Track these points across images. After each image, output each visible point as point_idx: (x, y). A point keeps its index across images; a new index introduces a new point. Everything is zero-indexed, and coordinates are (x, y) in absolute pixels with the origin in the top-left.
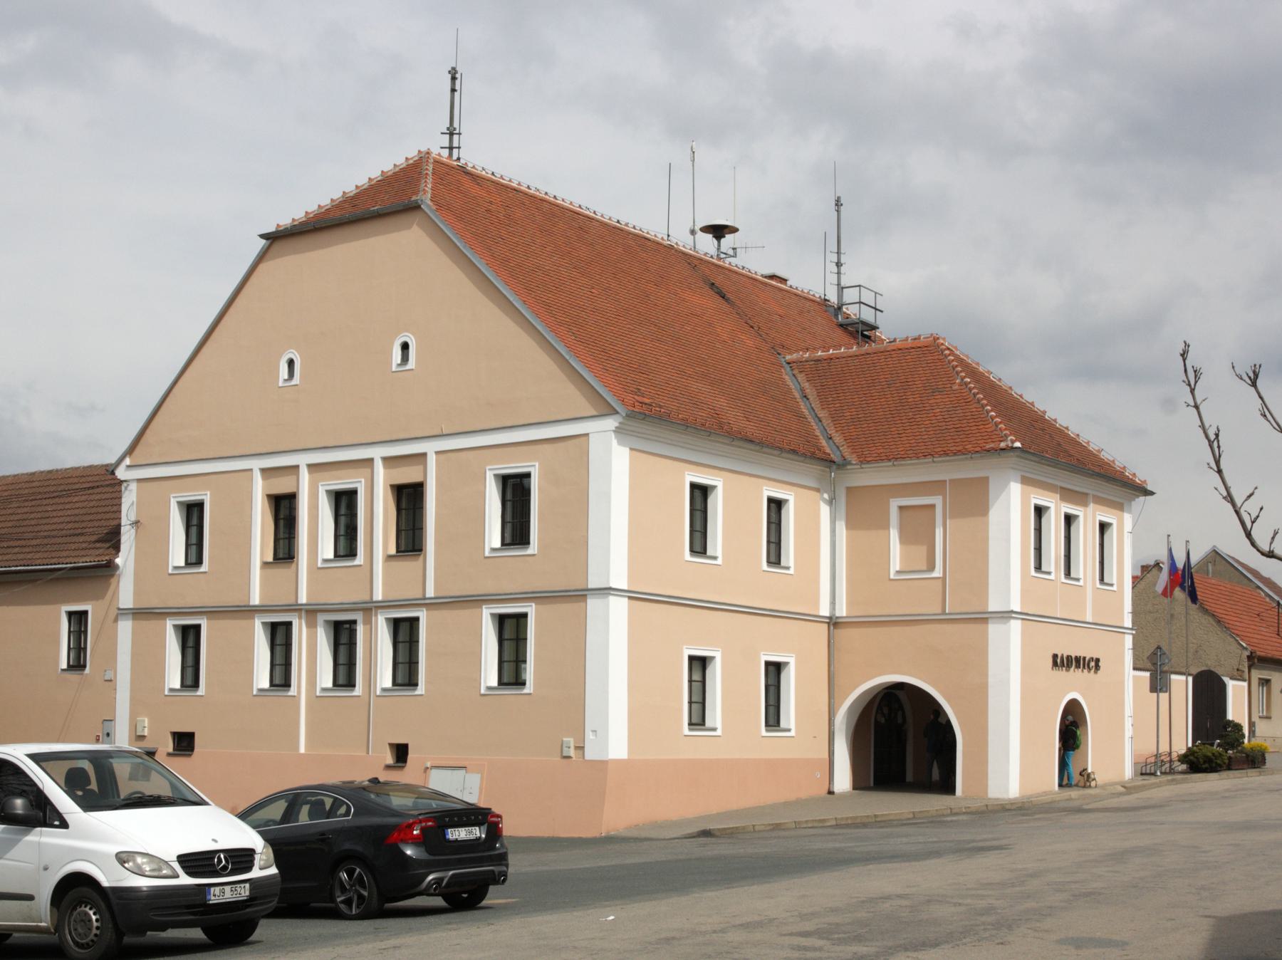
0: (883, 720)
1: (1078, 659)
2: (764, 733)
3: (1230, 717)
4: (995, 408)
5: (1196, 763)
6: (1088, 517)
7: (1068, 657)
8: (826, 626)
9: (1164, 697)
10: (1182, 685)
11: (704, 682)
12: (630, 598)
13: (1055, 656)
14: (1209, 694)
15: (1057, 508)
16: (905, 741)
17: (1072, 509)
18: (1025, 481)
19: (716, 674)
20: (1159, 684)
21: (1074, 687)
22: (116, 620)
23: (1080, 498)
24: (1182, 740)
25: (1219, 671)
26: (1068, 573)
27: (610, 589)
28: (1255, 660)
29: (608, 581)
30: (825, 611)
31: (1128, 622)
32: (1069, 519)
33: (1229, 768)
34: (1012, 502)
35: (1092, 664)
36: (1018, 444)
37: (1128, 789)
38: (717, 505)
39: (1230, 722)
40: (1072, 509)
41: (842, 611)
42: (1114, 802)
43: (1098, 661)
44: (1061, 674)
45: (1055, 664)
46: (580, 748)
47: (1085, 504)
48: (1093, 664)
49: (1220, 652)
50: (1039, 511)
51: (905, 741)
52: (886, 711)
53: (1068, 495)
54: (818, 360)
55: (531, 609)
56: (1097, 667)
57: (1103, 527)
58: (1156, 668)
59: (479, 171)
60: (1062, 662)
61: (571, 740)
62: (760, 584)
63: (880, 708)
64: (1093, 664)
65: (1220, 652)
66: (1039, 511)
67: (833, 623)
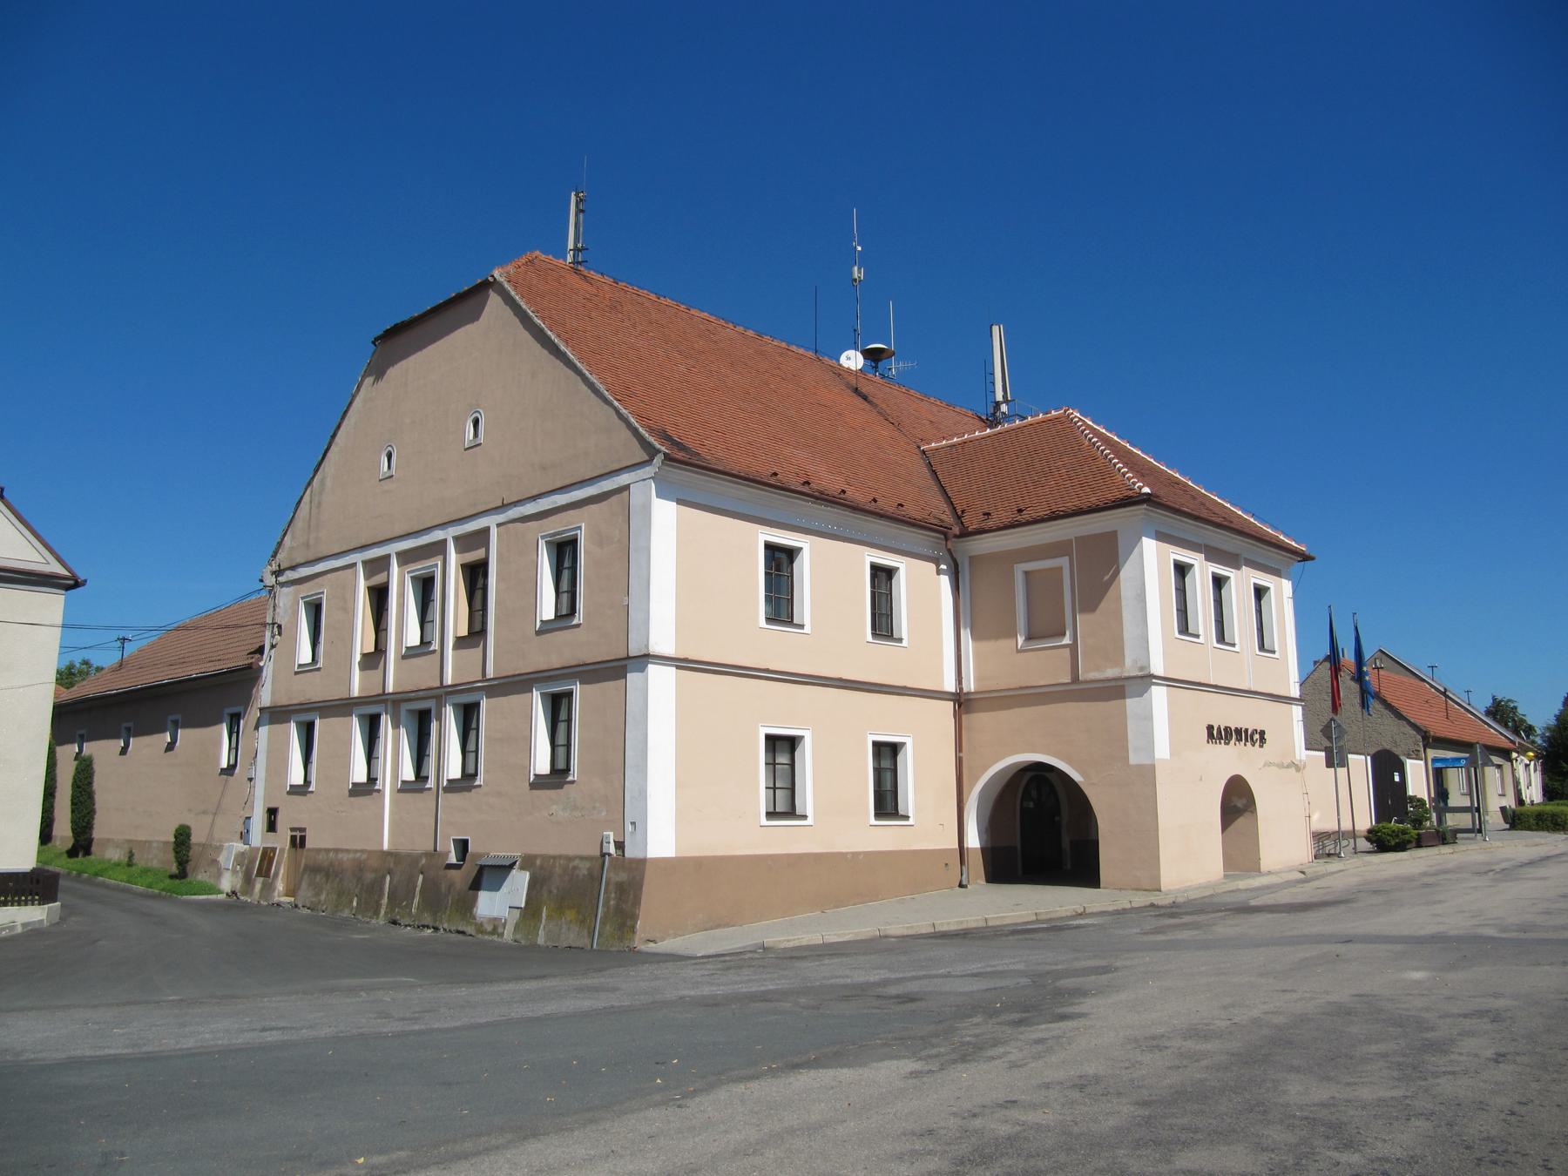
0: (1031, 805)
1: (1238, 731)
2: (873, 821)
3: (1410, 792)
4: (1131, 469)
5: (1381, 842)
6: (1242, 581)
7: (1226, 729)
8: (949, 706)
9: (1342, 771)
10: (1360, 765)
11: (792, 765)
12: (678, 667)
13: (1210, 728)
14: (1386, 768)
15: (1203, 570)
16: (1041, 829)
17: (1222, 571)
18: (1161, 537)
19: (807, 756)
20: (1335, 759)
21: (1232, 760)
22: (257, 728)
23: (1234, 561)
24: (1365, 819)
25: (1396, 751)
26: (1221, 637)
27: (647, 656)
28: (1431, 741)
29: (647, 646)
30: (950, 686)
31: (1295, 692)
32: (1219, 582)
33: (1419, 846)
34: (1152, 560)
35: (1257, 736)
36: (1146, 490)
37: (1305, 877)
38: (805, 570)
39: (1412, 799)
40: (1222, 571)
41: (970, 685)
42: (1284, 897)
43: (1262, 733)
44: (1220, 748)
45: (1210, 735)
46: (620, 846)
47: (1238, 568)
48: (1258, 737)
49: (1390, 734)
50: (1182, 570)
51: (1041, 829)
52: (1034, 793)
53: (1213, 554)
54: (953, 446)
55: (577, 689)
56: (1263, 740)
57: (1260, 592)
58: (1331, 743)
59: (1453, 933)
60: (1218, 735)
61: (612, 834)
62: (877, 661)
63: (1026, 794)
64: (1258, 737)
65: (1390, 734)
66: (1182, 570)
67: (962, 702)
